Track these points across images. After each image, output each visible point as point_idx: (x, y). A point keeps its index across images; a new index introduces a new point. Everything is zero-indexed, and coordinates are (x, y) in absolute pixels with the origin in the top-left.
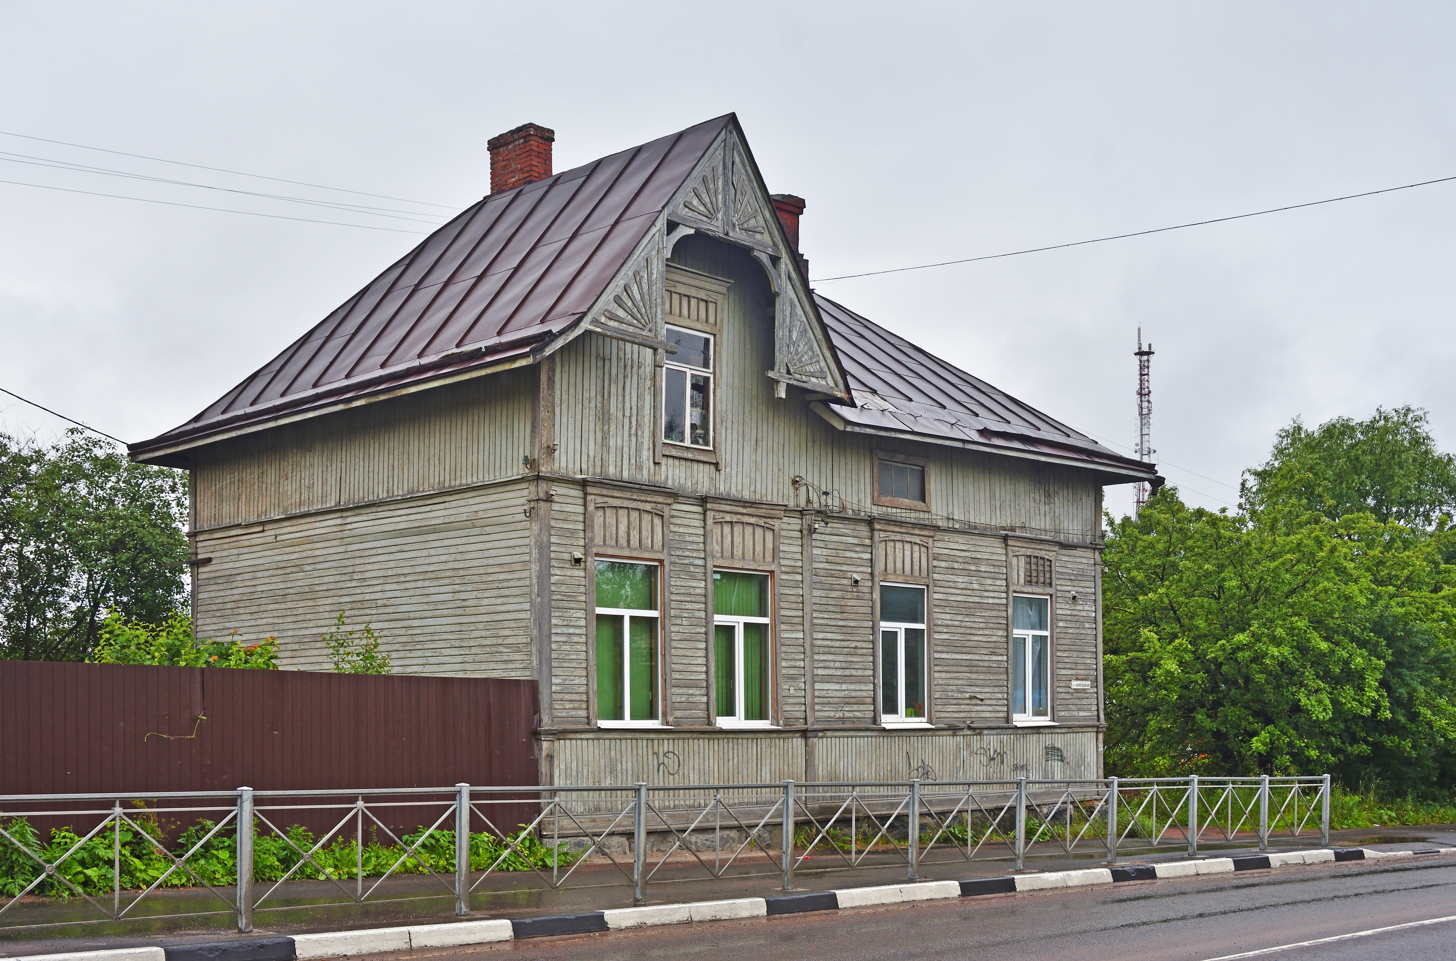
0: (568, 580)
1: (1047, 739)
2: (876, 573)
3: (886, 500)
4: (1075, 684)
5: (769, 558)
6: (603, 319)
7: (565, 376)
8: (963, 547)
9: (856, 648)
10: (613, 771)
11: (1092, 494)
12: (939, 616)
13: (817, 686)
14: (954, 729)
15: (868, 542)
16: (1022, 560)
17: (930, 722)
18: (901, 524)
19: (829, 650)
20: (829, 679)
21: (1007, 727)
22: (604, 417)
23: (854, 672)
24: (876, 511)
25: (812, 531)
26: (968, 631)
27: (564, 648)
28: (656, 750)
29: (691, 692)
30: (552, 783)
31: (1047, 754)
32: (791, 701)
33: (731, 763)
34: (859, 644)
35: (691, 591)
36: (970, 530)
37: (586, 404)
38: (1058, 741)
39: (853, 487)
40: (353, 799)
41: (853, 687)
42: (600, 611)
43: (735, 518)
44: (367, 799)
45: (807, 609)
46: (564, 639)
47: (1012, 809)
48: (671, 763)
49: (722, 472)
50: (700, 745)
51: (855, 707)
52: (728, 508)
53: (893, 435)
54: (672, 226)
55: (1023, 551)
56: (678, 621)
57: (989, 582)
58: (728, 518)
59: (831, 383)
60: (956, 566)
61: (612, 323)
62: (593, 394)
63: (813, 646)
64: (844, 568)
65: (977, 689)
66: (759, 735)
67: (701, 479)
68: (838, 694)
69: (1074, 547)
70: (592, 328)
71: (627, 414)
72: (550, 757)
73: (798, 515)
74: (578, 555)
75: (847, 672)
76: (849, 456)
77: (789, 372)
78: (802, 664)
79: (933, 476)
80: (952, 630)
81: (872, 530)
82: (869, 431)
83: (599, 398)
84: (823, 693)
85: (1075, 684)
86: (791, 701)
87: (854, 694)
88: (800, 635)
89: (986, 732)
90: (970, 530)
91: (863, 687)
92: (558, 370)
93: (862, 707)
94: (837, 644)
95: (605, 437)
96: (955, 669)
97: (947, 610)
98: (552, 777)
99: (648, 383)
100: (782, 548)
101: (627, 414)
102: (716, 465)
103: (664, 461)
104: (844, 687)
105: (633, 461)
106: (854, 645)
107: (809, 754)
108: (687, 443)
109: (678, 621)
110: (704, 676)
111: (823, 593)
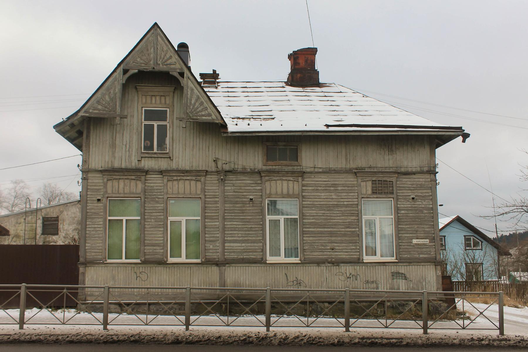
1: (394, 269)
3: (270, 163)
4: (415, 241)
5: (199, 192)
6: (91, 111)
8: (325, 180)
9: (251, 228)
10: (114, 278)
12: (306, 212)
14: (319, 263)
19: (234, 229)
22: (113, 146)
23: (250, 238)
26: (329, 218)
27: (92, 232)
28: (135, 271)
29: (155, 248)
31: (393, 276)
32: (211, 251)
33: (176, 277)
34: (253, 226)
35: (157, 208)
38: (402, 269)
39: (253, 159)
40: (63, 288)
41: (249, 245)
43: (179, 178)
44: (68, 289)
46: (92, 229)
48: (144, 276)
49: (174, 160)
50: (160, 269)
51: (251, 254)
52: (174, 174)
54: (125, 71)
56: (149, 220)
57: (345, 194)
58: (175, 178)
60: (320, 188)
64: (245, 194)
65: (336, 245)
66: (191, 265)
67: (163, 164)
68: (240, 248)
69: (414, 173)
70: (84, 114)
71: (124, 143)
72: (84, 274)
74: (99, 198)
82: (237, 134)
84: (230, 248)
85: (415, 241)
86: (211, 251)
87: (249, 248)
88: (218, 223)
92: (92, 131)
93: (255, 254)
94: (240, 226)
95: (113, 153)
96: (319, 235)
97: (314, 209)
101: (124, 143)
102: (170, 158)
104: (243, 245)
106: (250, 226)
107: (222, 276)
109: (149, 220)
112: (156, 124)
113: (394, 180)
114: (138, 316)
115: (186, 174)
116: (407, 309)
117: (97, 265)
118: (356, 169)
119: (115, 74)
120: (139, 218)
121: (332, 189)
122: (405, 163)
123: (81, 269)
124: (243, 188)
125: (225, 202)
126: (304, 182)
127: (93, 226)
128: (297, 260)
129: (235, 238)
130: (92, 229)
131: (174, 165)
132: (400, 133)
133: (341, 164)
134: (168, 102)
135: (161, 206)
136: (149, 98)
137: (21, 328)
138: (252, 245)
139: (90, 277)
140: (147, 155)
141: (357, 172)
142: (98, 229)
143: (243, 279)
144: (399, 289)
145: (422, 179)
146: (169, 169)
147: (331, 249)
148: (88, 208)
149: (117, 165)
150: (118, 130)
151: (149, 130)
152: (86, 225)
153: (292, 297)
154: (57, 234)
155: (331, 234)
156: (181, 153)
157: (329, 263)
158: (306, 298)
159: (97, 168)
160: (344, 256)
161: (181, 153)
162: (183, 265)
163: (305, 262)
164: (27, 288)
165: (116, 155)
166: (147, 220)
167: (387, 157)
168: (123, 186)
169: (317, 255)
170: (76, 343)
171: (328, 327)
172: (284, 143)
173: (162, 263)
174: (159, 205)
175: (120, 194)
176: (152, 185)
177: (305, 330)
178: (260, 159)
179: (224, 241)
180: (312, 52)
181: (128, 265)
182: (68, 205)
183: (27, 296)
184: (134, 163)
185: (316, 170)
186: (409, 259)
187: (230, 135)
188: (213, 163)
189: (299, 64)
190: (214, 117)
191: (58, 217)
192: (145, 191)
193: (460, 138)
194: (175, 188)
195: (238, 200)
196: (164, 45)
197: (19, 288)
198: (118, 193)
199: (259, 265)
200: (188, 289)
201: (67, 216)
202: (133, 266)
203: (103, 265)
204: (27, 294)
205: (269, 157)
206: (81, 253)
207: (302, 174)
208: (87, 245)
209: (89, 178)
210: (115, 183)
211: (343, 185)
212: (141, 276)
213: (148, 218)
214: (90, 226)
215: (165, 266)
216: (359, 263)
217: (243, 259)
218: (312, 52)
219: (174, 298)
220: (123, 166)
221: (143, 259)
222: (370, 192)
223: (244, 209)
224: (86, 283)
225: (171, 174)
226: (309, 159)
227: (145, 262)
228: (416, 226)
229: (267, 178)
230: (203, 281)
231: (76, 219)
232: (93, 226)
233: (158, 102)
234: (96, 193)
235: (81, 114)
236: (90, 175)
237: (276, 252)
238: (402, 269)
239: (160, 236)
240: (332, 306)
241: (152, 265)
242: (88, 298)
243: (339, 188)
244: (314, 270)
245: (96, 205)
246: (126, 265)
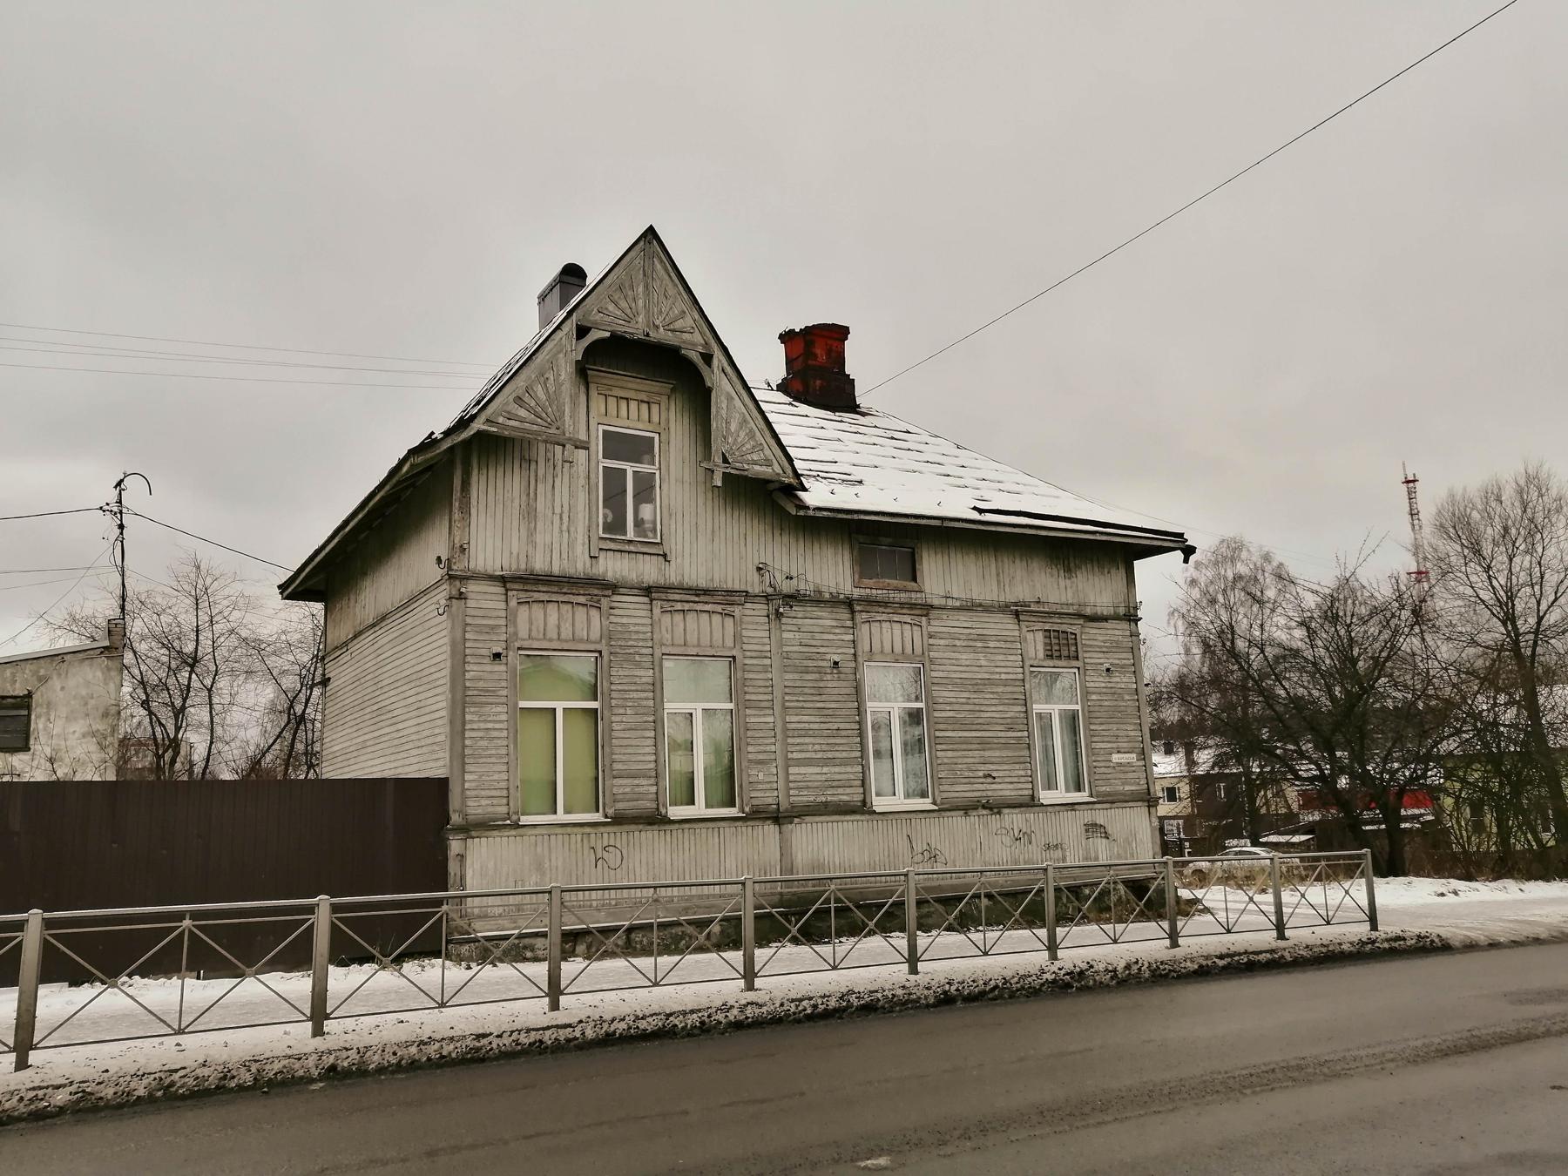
0: (486, 675)
1: (1087, 816)
2: (860, 653)
4: (1116, 758)
5: (729, 643)
6: (501, 420)
7: (483, 478)
10: (539, 868)
11: (1122, 572)
13: (792, 770)
14: (967, 808)
15: (849, 623)
16: (1040, 635)
17: (934, 803)
18: (885, 604)
19: (806, 733)
20: (808, 762)
21: (1031, 803)
22: (529, 514)
23: (838, 755)
24: (857, 593)
25: (779, 615)
27: (481, 743)
30: (463, 886)
34: (842, 726)
36: (971, 607)
37: (508, 503)
38: (1100, 817)
39: (830, 570)
40: (180, 916)
41: (837, 769)
42: (523, 704)
43: (687, 606)
44: (195, 916)
45: (778, 693)
46: (481, 734)
47: (1041, 890)
48: (613, 857)
50: (649, 836)
51: (840, 791)
52: (677, 597)
53: (855, 517)
54: (582, 332)
55: (1039, 626)
57: (1001, 657)
58: (679, 606)
59: (778, 469)
61: (512, 423)
62: (516, 493)
63: (785, 730)
64: (822, 650)
67: (648, 570)
68: (819, 777)
69: (1105, 619)
71: (558, 511)
72: (462, 857)
73: (763, 600)
74: (499, 650)
75: (830, 755)
76: (952, 555)
77: (725, 460)
78: (773, 748)
79: (925, 555)
80: (956, 707)
81: (853, 612)
82: (913, 521)
83: (524, 498)
84: (799, 778)
85: (1116, 758)
88: (771, 719)
89: (1006, 811)
90: (971, 607)
91: (849, 769)
92: (475, 472)
93: (848, 790)
94: (816, 726)
95: (531, 533)
98: (463, 878)
99: (582, 481)
100: (745, 633)
101: (558, 511)
102: (665, 556)
103: (603, 554)
104: (825, 770)
105: (565, 556)
108: (631, 535)
109: (621, 711)
110: (652, 765)
111: (796, 676)
112: (630, 468)
113: (1076, 629)
114: (635, 961)
115: (702, 598)
116: (1113, 898)
117: (496, 833)
118: (1016, 604)
119: (559, 334)
120: (731, 706)
121: (979, 644)
122: (1092, 599)
123: (455, 846)
124: (818, 636)
125: (785, 669)
126: (931, 629)
127: (482, 726)
128: (925, 804)
129: (808, 755)
130: (481, 734)
131: (672, 575)
132: (1098, 537)
133: (987, 592)
134: (655, 419)
135: (646, 675)
136: (612, 402)
138: (843, 769)
139: (477, 866)
140: (612, 546)
141: (1018, 612)
142: (495, 734)
143: (830, 852)
144: (1097, 859)
145: (1118, 630)
146: (662, 582)
147: (985, 776)
148: (468, 676)
149: (539, 565)
150: (541, 472)
151: (614, 479)
152: (464, 723)
153: (954, 888)
154: (26, 748)
155: (984, 744)
156: (687, 545)
157: (984, 807)
158: (827, 901)
159: (490, 571)
160: (1007, 793)
161: (687, 545)
162: (710, 825)
163: (945, 808)
165: (539, 538)
166: (616, 711)
167: (1062, 583)
168: (546, 621)
169: (963, 792)
170: (750, 1026)
172: (889, 540)
173: (656, 819)
174: (642, 673)
175: (551, 640)
176: (624, 620)
178: (848, 572)
179: (788, 762)
180: (836, 334)
181: (576, 830)
183: (46, 947)
184: (580, 564)
185: (950, 603)
186: (1109, 794)
187: (811, 513)
188: (756, 575)
189: (816, 356)
190: (778, 469)
191: (30, 695)
192: (609, 636)
193: (1179, 555)
194: (679, 629)
195: (810, 663)
196: (670, 284)
197: (20, 926)
198: (699, 645)
199: (858, 817)
201: (61, 694)
202: (588, 830)
203: (513, 832)
204: (333, 925)
205: (864, 568)
206: (454, 802)
207: (927, 609)
208: (467, 777)
209: (470, 595)
210: (537, 610)
211: (998, 639)
212: (606, 855)
213: (617, 706)
214: (475, 726)
215: (667, 827)
216: (863, 813)
217: (826, 804)
218: (836, 334)
219: (686, 910)
220: (556, 570)
221: (610, 812)
222: (1041, 654)
223: (822, 684)
225: (671, 597)
226: (942, 576)
227: (619, 820)
228: (1115, 727)
229: (864, 615)
230: (742, 862)
231: (92, 702)
232: (482, 726)
233: (624, 412)
234: (486, 637)
235: (477, 426)
236: (472, 588)
237: (1051, 784)
238: (1100, 817)
239: (648, 750)
240: (1015, 905)
241: (633, 827)
242: (477, 925)
243: (991, 644)
244: (957, 822)
245: (488, 668)
246: (569, 830)
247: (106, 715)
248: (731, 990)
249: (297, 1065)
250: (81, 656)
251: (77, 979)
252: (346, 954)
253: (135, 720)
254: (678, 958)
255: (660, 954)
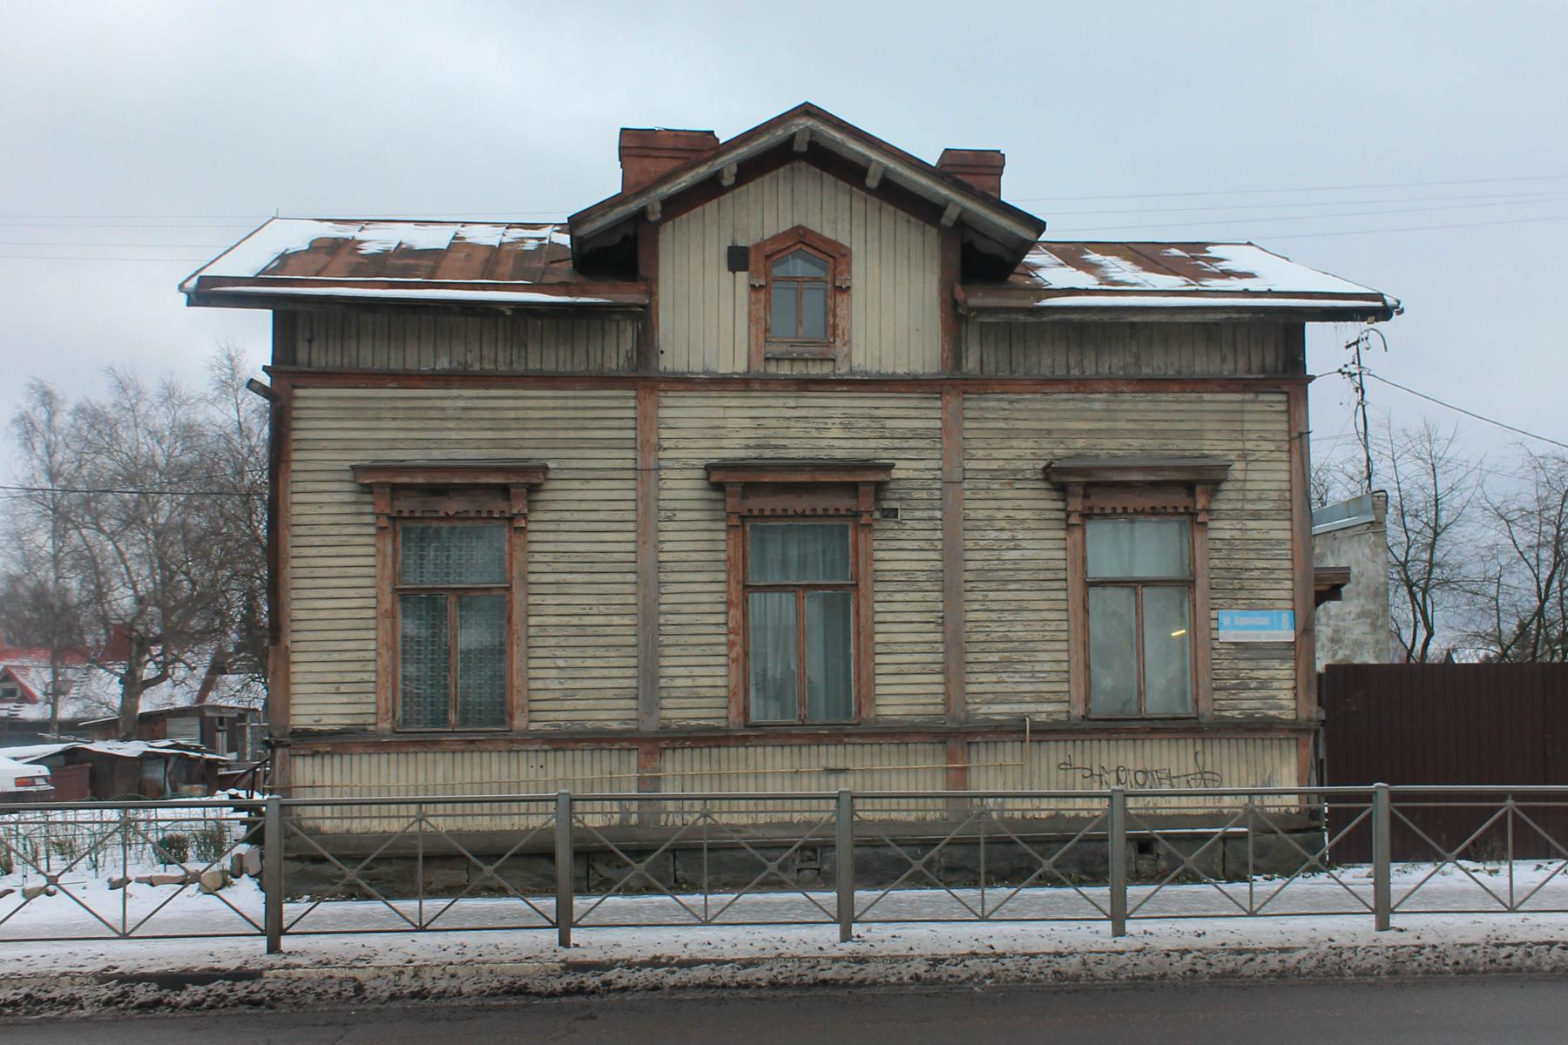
40: (1502, 796)
44: (1518, 796)
114: (394, 903)
137: (1119, 931)
164: (1394, 797)
171: (496, 934)
177: (425, 946)
182: (1338, 534)
200: (563, 801)
224: (974, 783)
247: (1376, 594)
248: (1091, 935)
249: (1142, 960)
250: (1350, 532)
251: (1427, 855)
252: (1408, 849)
253: (18, 553)
254: (1153, 888)
255: (989, 884)
